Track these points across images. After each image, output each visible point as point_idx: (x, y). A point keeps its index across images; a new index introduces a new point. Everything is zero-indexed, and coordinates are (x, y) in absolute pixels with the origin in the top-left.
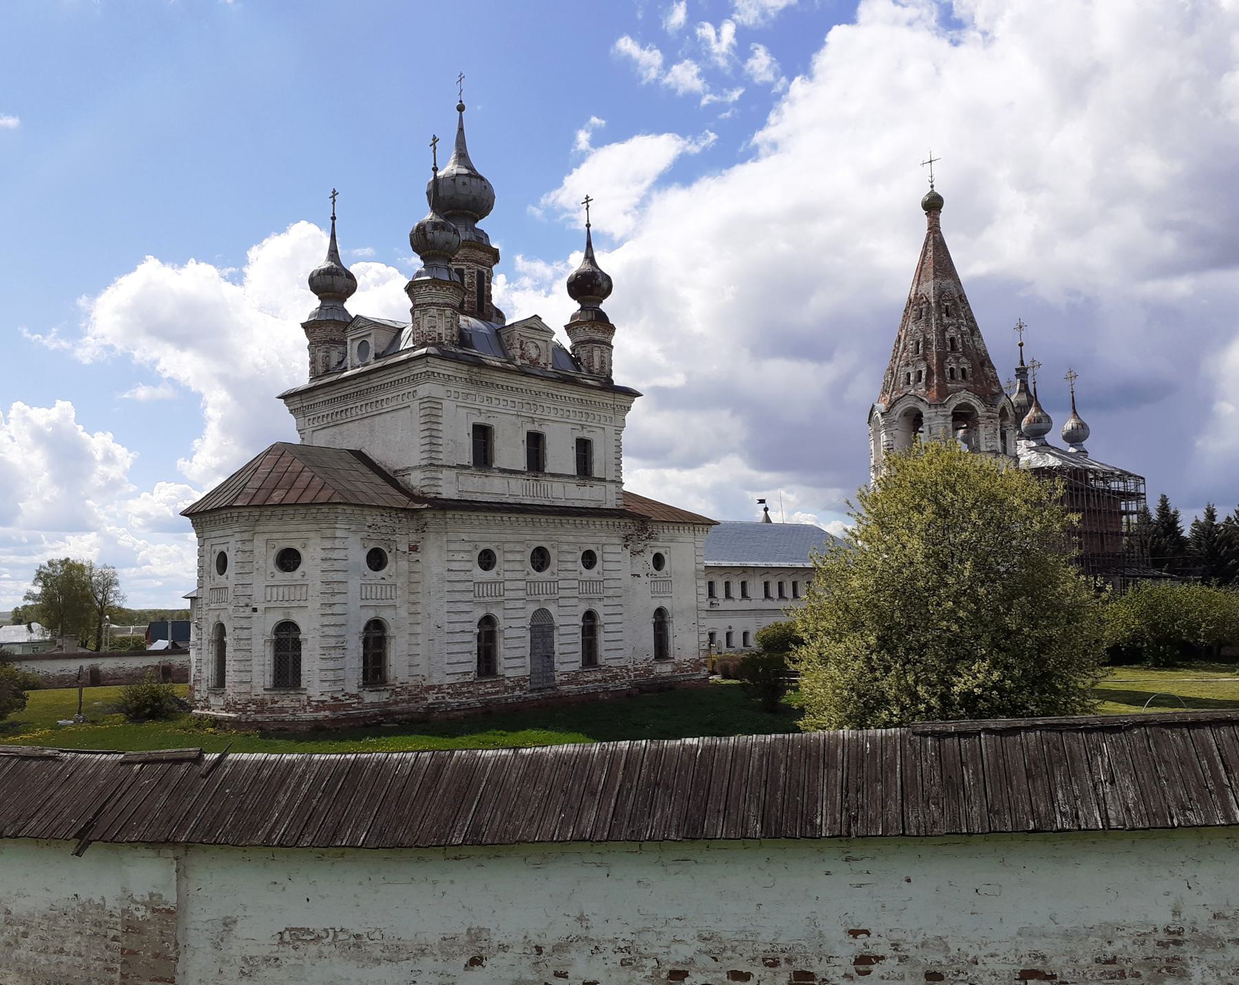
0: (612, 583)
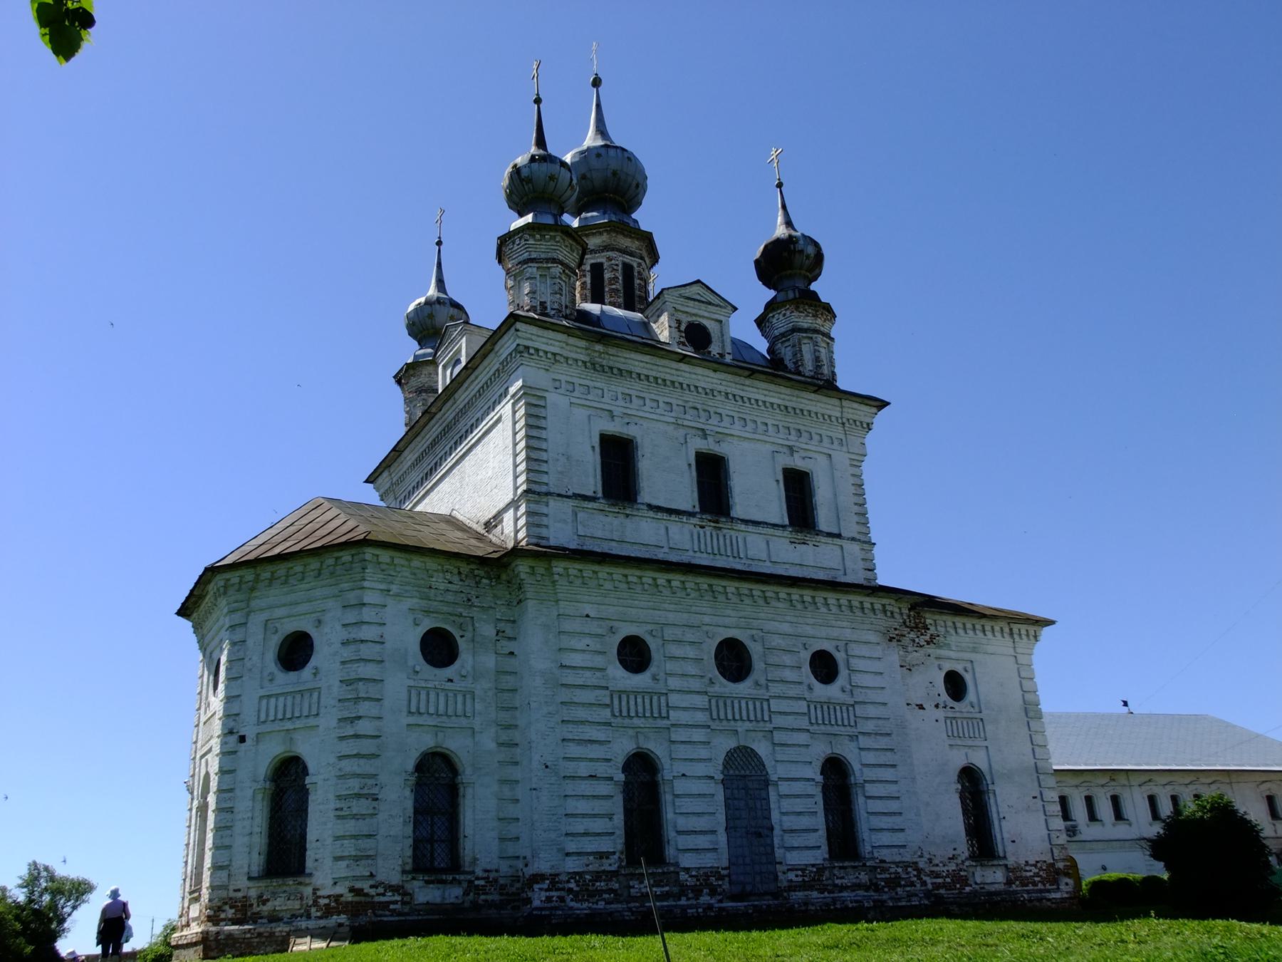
0: (872, 711)
